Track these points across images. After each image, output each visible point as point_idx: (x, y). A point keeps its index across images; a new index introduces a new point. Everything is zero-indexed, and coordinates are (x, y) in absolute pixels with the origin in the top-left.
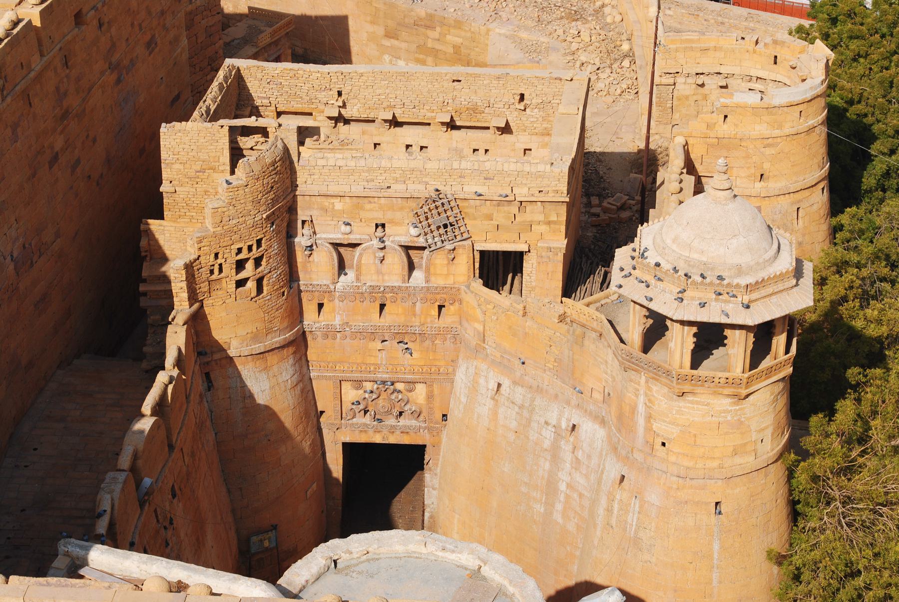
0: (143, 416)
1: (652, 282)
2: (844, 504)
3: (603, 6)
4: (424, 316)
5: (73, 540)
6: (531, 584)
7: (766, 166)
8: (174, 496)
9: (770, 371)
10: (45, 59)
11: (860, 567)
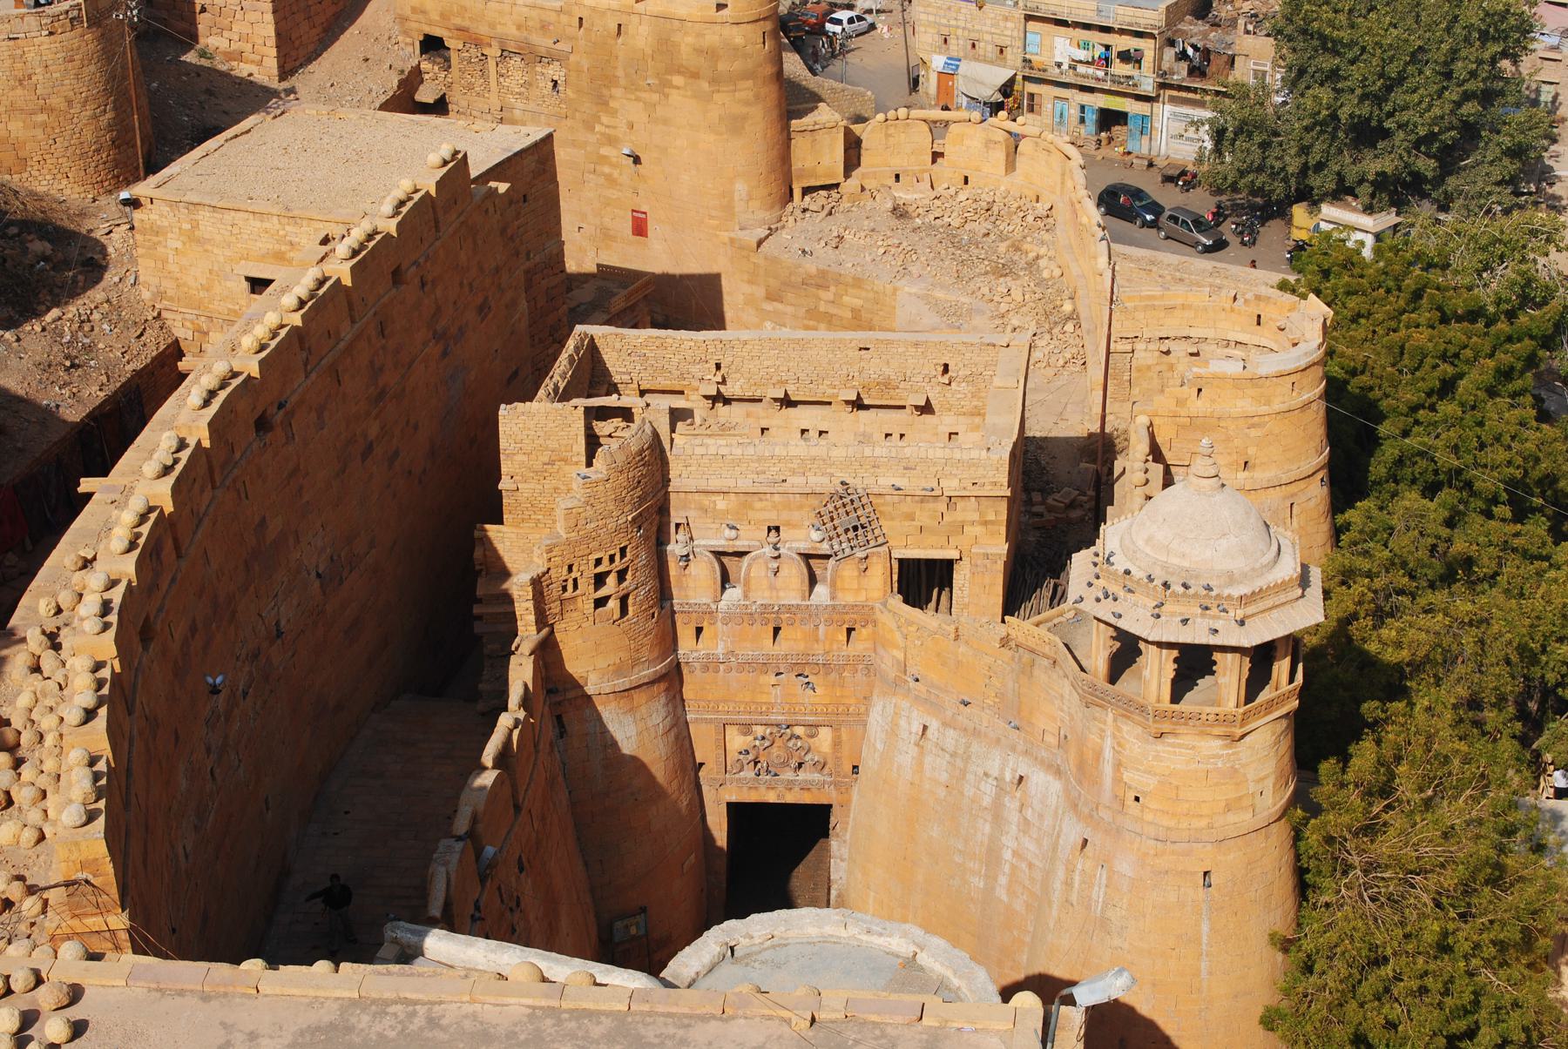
0: (485, 768)
1: (1121, 594)
2: (1366, 872)
3: (1037, 257)
4: (830, 642)
5: (402, 923)
6: (981, 975)
7: (1252, 451)
8: (521, 869)
9: (1270, 705)
10: (357, 326)
11: (1389, 952)
